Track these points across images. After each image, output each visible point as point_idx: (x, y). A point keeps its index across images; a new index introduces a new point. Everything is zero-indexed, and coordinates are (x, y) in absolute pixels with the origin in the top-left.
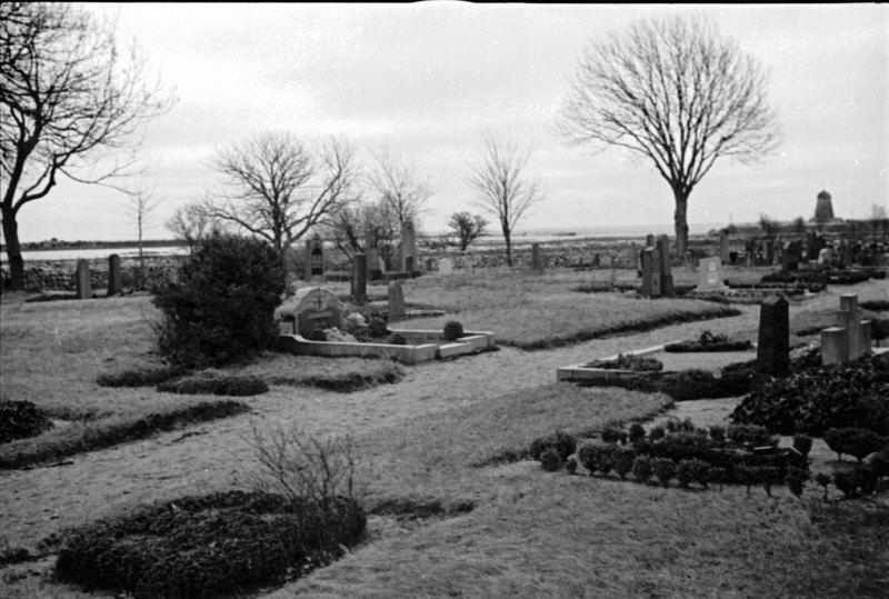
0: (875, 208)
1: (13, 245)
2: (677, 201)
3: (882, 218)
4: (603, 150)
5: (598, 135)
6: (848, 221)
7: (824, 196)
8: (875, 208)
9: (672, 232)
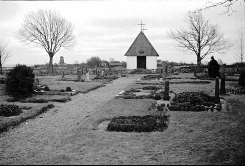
0: (75, 61)
1: (1, 68)
2: (50, 58)
3: (77, 63)
4: (29, 44)
5: (28, 39)
6: (68, 64)
7: (62, 57)
8: (75, 61)
9: (196, 63)
